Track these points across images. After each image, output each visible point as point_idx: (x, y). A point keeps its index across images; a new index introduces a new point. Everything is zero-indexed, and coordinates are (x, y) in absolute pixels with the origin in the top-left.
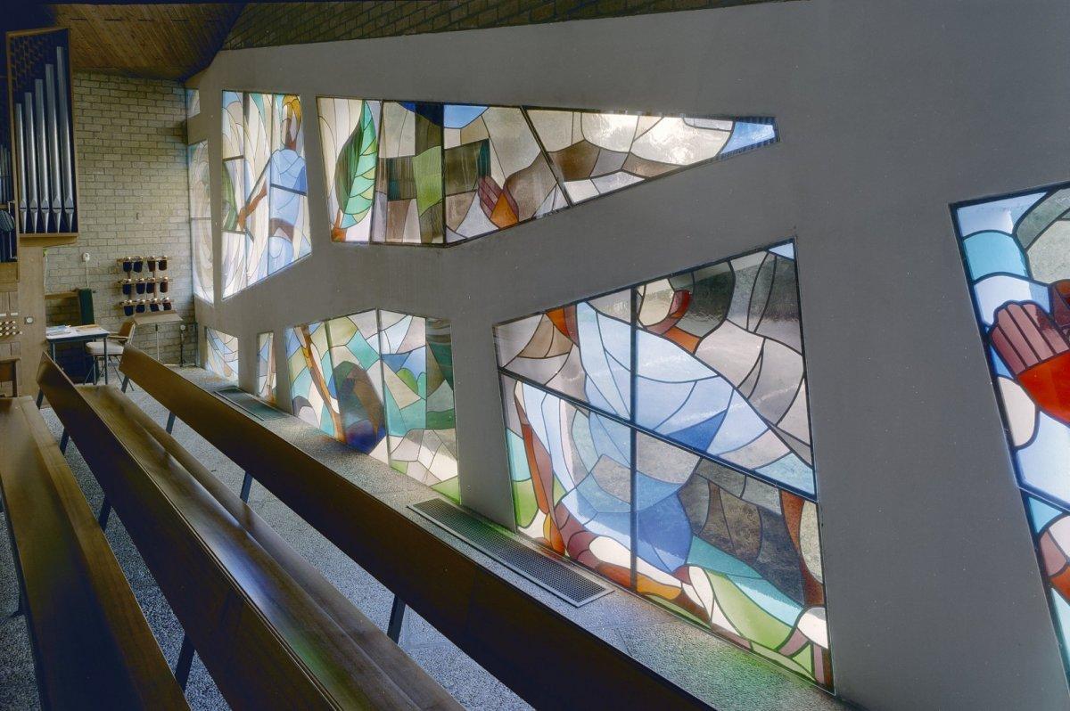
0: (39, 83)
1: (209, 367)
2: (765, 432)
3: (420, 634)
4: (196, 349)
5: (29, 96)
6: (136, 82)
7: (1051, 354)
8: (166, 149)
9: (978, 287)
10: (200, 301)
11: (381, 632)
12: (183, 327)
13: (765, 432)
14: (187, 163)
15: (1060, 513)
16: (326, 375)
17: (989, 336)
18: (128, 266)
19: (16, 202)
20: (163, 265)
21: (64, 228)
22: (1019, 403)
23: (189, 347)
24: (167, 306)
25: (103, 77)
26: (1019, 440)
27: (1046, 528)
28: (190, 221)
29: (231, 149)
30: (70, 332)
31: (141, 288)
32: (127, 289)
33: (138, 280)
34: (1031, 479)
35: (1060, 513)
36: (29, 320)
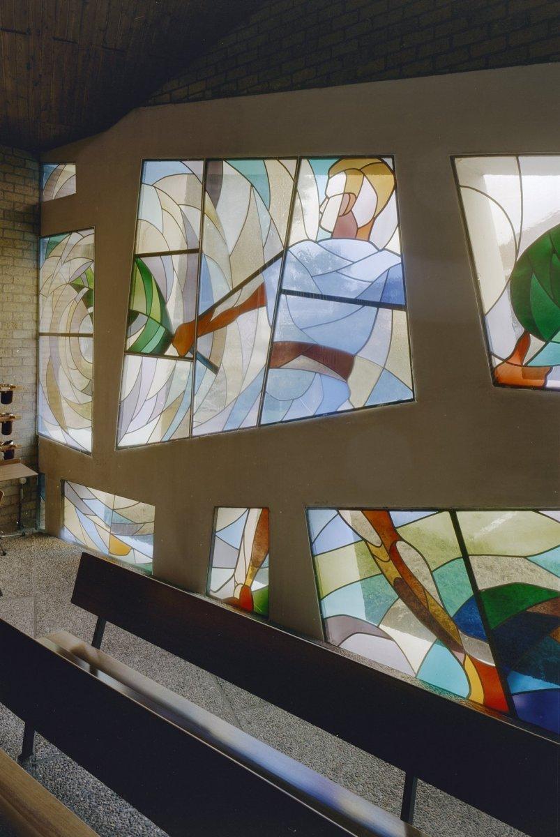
1: (66, 534)
8: (14, 240)
9: (316, 558)
10: (54, 447)
14: (38, 260)
28: (38, 335)
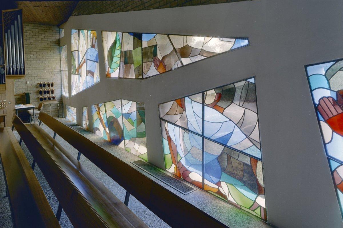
0: (12, 26)
1: (67, 118)
2: (245, 138)
4: (63, 112)
5: (9, 31)
6: (44, 26)
7: (337, 114)
8: (53, 48)
9: (314, 92)
10: (64, 96)
11: (122, 203)
12: (59, 105)
13: (245, 138)
14: (60, 52)
15: (340, 164)
16: (105, 120)
17: (317, 108)
18: (41, 85)
19: (5, 65)
20: (52, 85)
21: (21, 73)
22: (327, 129)
23: (60, 111)
24: (54, 98)
25: (33, 25)
26: (327, 141)
27: (335, 169)
28: (61, 71)
29: (74, 48)
30: (23, 106)
31: (45, 92)
32: (41, 93)
33: (44, 90)
34: (331, 154)
35: (340, 164)
36: (9, 103)
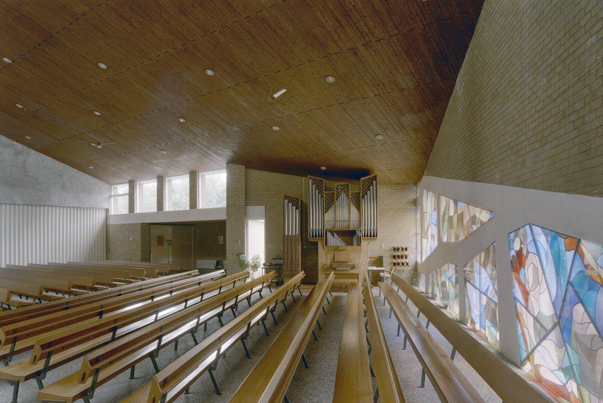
3: (409, 301)
4: (417, 281)
12: (413, 272)
16: (442, 281)
18: (394, 249)
20: (406, 249)
21: (374, 236)
23: (414, 279)
25: (390, 186)
29: (425, 210)
30: (375, 268)
31: (398, 257)
32: (394, 257)
33: (398, 254)
